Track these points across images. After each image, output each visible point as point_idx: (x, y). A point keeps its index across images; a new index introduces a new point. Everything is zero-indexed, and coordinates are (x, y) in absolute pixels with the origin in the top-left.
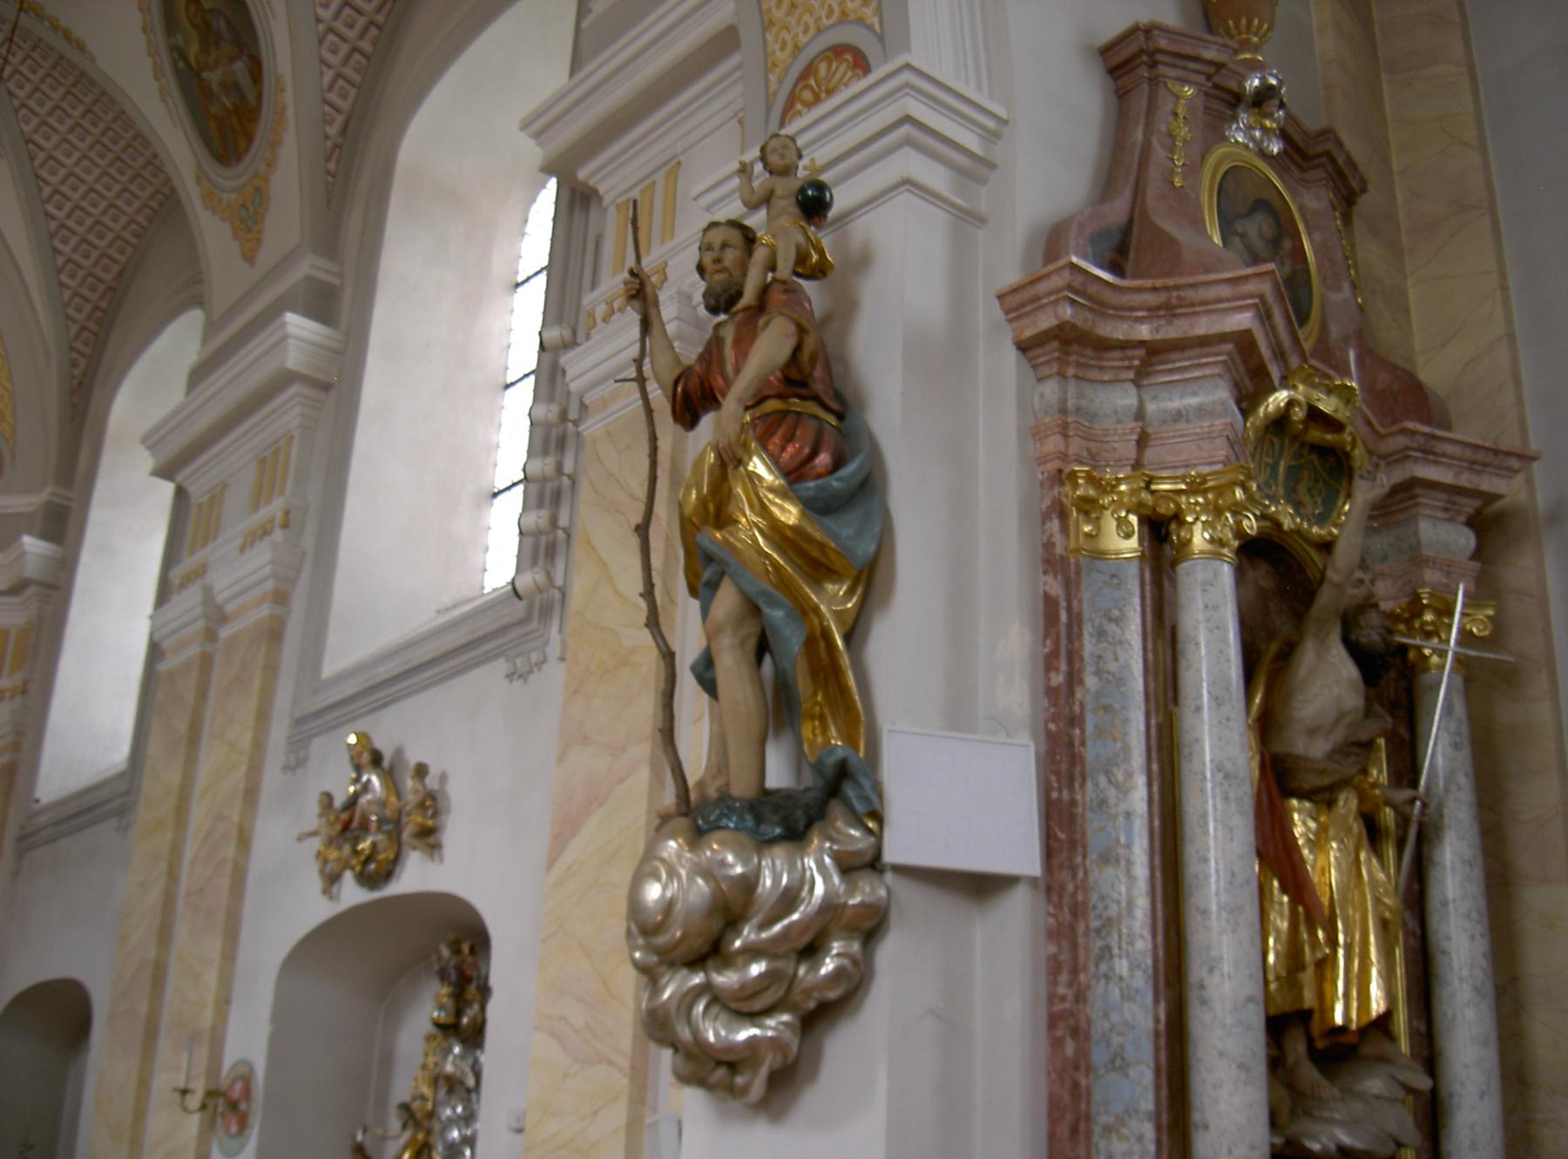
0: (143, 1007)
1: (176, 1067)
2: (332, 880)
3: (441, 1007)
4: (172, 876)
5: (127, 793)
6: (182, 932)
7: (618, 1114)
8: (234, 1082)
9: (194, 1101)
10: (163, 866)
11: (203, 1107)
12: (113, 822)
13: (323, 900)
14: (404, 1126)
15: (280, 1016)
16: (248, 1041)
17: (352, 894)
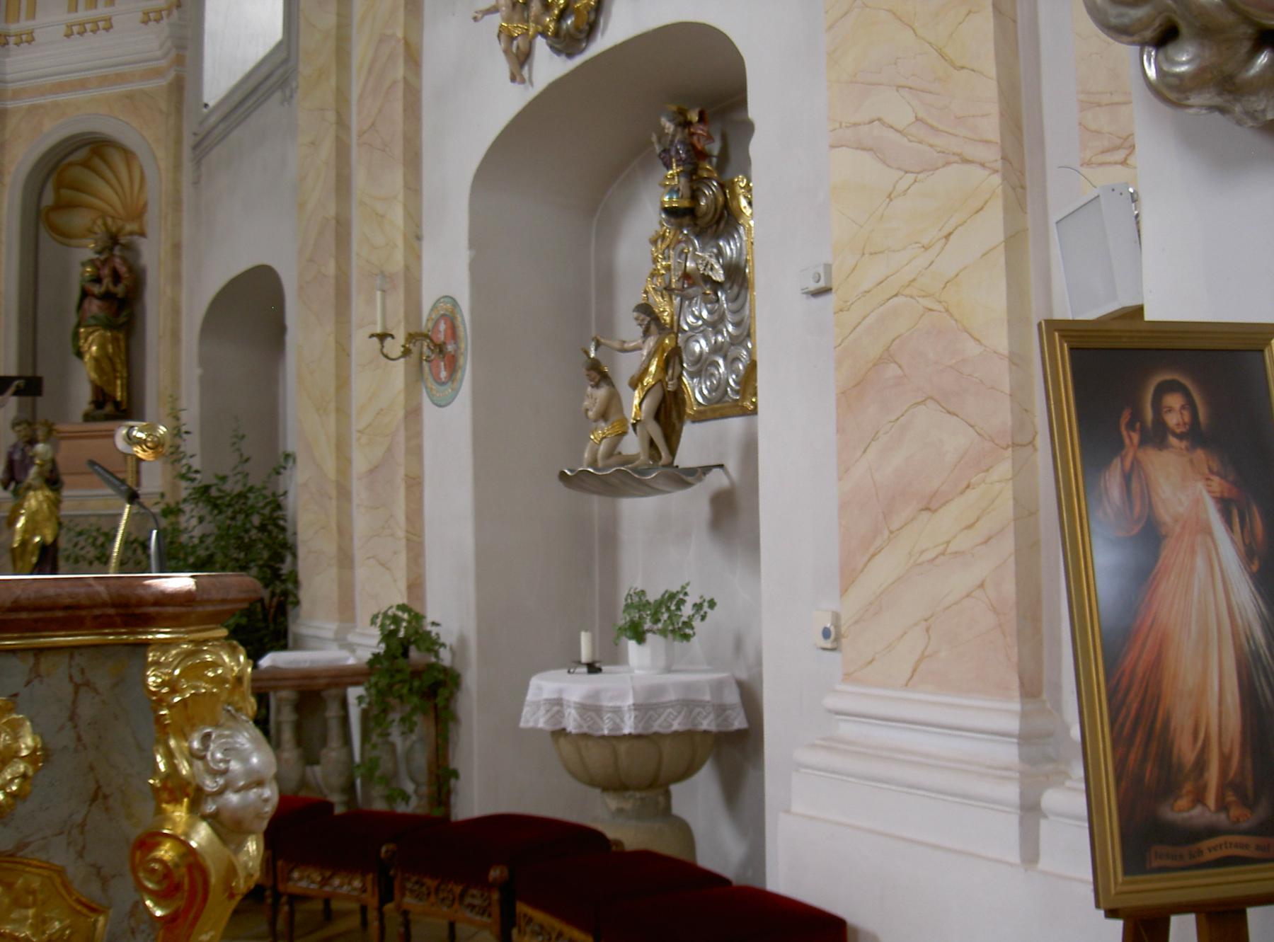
0: (331, 269)
1: (371, 312)
2: (521, 59)
3: (673, 190)
4: (342, 123)
5: (285, 61)
6: (360, 178)
7: (991, 228)
8: (436, 324)
9: (395, 347)
10: (331, 116)
11: (406, 353)
12: (278, 95)
13: (517, 87)
14: (646, 333)
15: (481, 240)
16: (447, 273)
17: (549, 67)
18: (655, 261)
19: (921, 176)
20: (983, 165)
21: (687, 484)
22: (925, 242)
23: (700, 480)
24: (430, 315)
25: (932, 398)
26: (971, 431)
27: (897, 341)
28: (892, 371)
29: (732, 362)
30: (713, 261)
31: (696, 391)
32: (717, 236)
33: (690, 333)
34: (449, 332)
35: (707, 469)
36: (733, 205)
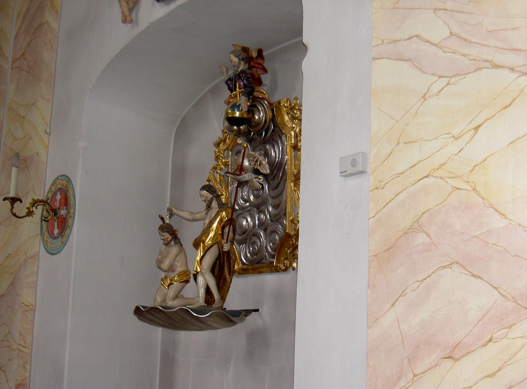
18: (217, 158)
19: (453, 80)
20: (512, 69)
21: (231, 323)
22: (456, 132)
23: (242, 320)
24: (50, 188)
25: (457, 263)
26: (495, 292)
27: (426, 215)
28: (421, 239)
29: (270, 233)
30: (261, 158)
31: (243, 254)
32: (265, 142)
33: (240, 212)
34: (63, 201)
35: (248, 312)
36: (279, 120)
